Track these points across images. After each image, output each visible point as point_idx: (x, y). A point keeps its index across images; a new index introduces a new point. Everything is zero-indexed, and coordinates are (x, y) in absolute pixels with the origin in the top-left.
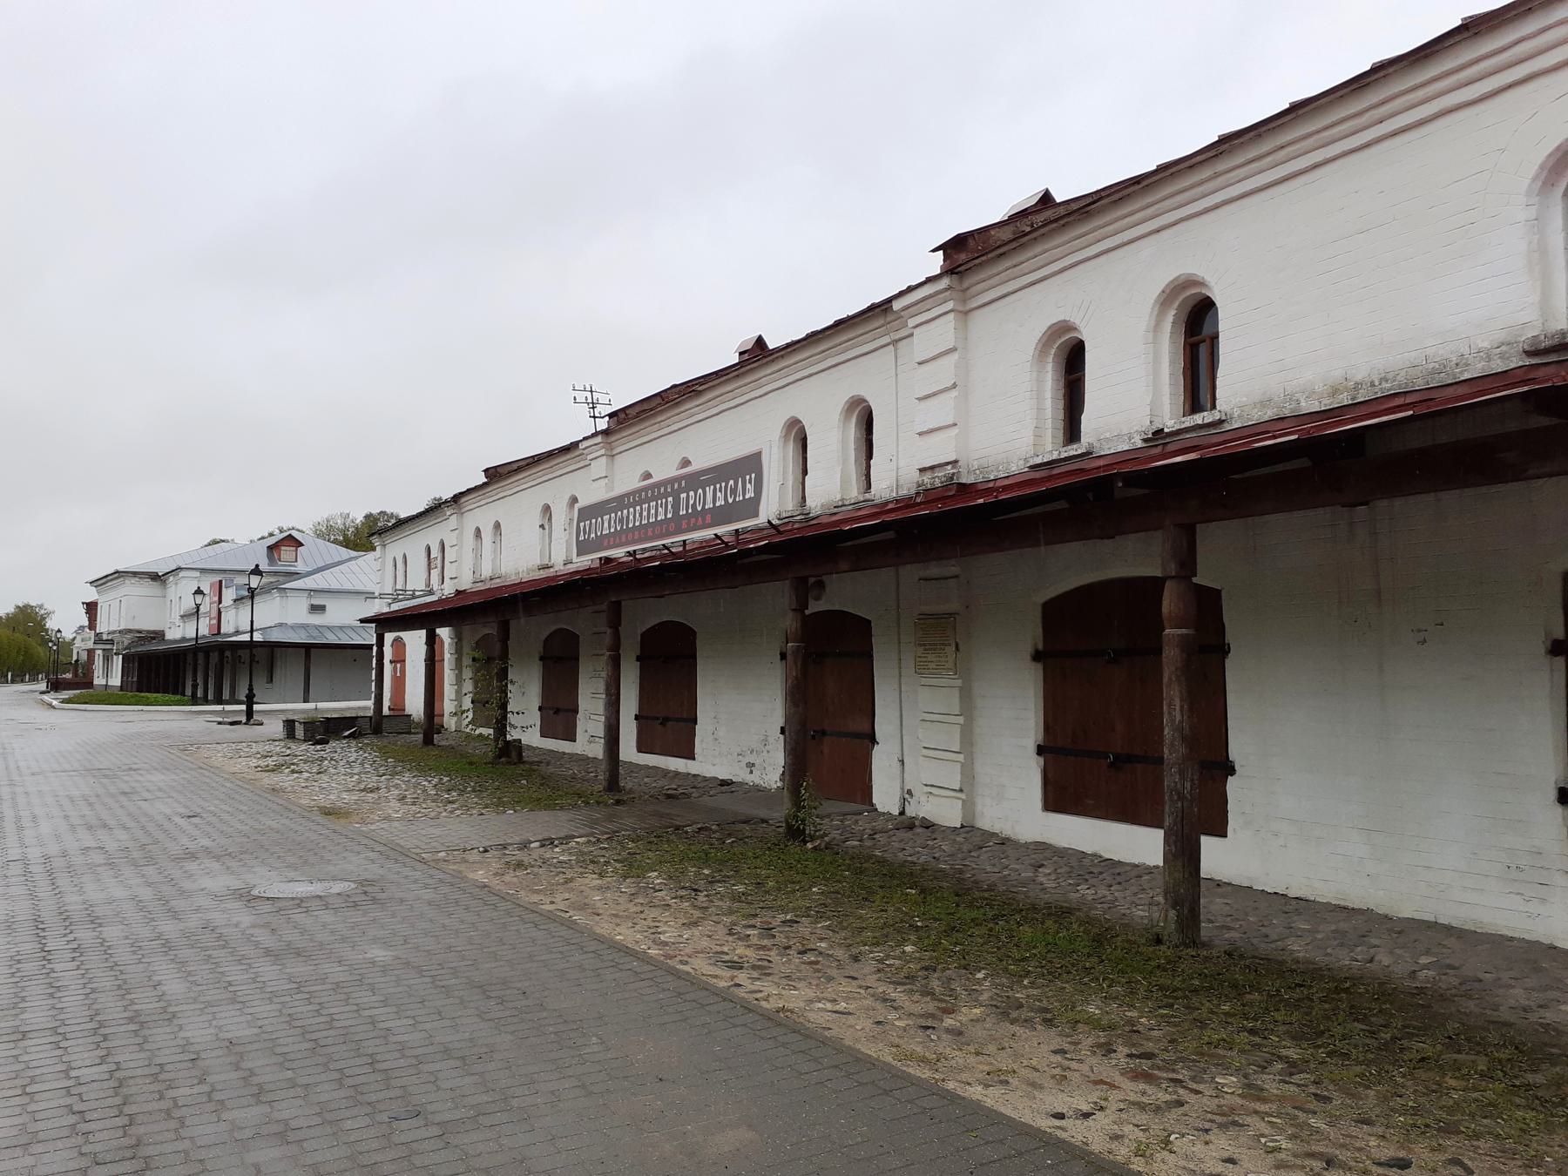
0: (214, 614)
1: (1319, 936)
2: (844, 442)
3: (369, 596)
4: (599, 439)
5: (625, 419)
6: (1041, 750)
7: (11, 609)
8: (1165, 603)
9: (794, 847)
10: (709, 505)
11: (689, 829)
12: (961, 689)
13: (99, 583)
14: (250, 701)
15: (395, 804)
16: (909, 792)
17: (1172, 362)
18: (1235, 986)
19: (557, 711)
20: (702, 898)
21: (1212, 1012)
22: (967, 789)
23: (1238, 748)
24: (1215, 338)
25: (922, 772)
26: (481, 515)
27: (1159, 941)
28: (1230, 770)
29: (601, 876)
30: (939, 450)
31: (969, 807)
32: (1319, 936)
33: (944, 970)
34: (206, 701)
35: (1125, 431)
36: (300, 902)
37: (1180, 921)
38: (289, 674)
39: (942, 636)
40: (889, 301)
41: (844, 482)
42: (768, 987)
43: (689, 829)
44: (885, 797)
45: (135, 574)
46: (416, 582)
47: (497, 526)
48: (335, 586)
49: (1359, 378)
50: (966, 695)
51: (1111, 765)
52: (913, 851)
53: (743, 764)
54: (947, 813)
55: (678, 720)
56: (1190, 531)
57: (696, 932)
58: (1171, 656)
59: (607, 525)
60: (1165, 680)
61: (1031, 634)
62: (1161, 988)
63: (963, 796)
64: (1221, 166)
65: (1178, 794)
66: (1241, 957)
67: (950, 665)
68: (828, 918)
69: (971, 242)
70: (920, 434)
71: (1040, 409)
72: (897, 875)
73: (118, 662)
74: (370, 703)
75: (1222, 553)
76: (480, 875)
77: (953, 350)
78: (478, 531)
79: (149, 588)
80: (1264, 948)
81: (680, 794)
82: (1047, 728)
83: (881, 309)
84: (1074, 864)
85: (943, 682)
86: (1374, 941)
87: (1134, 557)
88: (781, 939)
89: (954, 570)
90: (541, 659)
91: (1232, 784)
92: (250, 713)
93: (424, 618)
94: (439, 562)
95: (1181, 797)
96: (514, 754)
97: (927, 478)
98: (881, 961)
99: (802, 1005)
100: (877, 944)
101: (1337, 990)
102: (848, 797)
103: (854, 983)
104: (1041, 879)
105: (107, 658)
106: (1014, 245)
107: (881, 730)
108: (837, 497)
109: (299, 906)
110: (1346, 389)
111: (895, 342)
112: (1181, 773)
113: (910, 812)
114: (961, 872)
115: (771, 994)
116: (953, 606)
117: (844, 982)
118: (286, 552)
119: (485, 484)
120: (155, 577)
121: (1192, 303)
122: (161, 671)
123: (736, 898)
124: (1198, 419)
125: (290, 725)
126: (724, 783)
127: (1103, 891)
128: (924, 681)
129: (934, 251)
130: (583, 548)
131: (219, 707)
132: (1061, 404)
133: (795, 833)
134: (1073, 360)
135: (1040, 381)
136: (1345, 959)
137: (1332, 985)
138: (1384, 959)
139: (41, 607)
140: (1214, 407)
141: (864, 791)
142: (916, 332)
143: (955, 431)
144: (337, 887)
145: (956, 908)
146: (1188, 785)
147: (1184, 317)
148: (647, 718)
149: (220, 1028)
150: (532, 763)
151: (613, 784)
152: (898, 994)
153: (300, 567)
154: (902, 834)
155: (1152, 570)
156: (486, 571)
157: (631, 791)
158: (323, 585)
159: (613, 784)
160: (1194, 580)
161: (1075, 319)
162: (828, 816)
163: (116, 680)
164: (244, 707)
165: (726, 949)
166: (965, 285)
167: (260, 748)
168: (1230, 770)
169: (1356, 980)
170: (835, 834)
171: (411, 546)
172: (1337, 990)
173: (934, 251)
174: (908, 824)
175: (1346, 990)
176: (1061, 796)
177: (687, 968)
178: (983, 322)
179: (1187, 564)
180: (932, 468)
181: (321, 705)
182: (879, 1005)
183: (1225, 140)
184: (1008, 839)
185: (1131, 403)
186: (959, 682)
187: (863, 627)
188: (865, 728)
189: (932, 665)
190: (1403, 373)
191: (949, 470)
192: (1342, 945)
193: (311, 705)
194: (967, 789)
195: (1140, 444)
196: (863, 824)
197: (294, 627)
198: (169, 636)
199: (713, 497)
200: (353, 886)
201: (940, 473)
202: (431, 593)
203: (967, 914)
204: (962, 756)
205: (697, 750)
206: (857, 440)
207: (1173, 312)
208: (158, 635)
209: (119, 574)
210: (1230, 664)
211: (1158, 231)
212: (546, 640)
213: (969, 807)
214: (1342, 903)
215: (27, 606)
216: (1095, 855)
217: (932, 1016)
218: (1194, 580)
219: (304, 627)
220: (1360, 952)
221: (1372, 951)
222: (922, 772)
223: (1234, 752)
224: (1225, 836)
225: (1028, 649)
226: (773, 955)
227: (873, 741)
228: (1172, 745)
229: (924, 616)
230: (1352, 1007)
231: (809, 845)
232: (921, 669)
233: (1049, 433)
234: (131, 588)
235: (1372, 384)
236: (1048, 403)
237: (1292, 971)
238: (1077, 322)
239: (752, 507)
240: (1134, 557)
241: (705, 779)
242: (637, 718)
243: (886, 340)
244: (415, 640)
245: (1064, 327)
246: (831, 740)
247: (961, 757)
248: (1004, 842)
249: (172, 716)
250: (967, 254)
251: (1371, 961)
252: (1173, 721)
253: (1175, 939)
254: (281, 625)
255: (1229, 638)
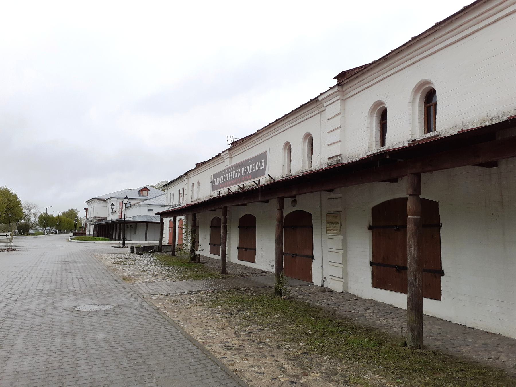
0: (120, 212)
1: (477, 345)
2: (303, 149)
3: (164, 206)
4: (227, 152)
5: (235, 144)
6: (371, 264)
7: (67, 211)
8: (408, 205)
9: (277, 298)
10: (251, 172)
11: (242, 289)
12: (342, 240)
13: (88, 202)
14: (124, 240)
15: (149, 276)
16: (325, 278)
17: (420, 114)
18: (433, 369)
19: (215, 245)
20: (232, 317)
21: (420, 382)
22: (345, 277)
23: (445, 265)
24: (435, 104)
25: (329, 271)
26: (194, 179)
27: (405, 345)
28: (443, 274)
29: (201, 306)
30: (334, 151)
31: (345, 284)
32: (477, 345)
33: (312, 354)
34: (115, 240)
35: (402, 141)
36: (89, 313)
37: (414, 337)
38: (141, 232)
39: (336, 220)
40: (317, 97)
41: (303, 163)
42: (237, 359)
43: (242, 289)
44: (317, 280)
45: (98, 199)
46: (176, 202)
47: (198, 182)
48: (156, 203)
49: (493, 115)
50: (344, 242)
51: (397, 270)
52: (321, 301)
53: (270, 265)
54: (337, 286)
55: (250, 249)
56: (418, 176)
57: (222, 332)
58: (410, 227)
59: (221, 180)
60: (408, 237)
61: (368, 219)
62: (401, 368)
63: (343, 280)
64: (437, 36)
65: (413, 284)
66: (440, 354)
67: (338, 231)
68: (276, 329)
69: (347, 75)
70: (328, 145)
71: (371, 134)
72: (310, 310)
73: (93, 227)
74: (158, 242)
75: (435, 187)
76: (159, 305)
77: (340, 114)
78: (193, 184)
79: (102, 204)
80: (452, 350)
81: (246, 275)
82: (373, 256)
83: (314, 101)
84: (381, 308)
85: (337, 237)
86: (501, 349)
87: (401, 190)
88: (253, 337)
89: (340, 195)
90: (210, 227)
91: (443, 279)
92: (124, 244)
93: (173, 213)
94: (182, 195)
95: (414, 285)
96: (197, 260)
97: (330, 161)
98: (288, 349)
99: (246, 368)
100: (290, 341)
101: (479, 373)
102: (304, 279)
103: (273, 359)
104: (366, 315)
105: (90, 226)
106: (360, 73)
107: (317, 253)
108: (300, 169)
109: (88, 314)
110: (488, 120)
111: (321, 112)
112: (415, 275)
113: (325, 286)
114: (335, 311)
115: (236, 362)
116: (340, 209)
117: (268, 357)
118: (144, 193)
119: (195, 169)
120: (104, 200)
121: (427, 91)
122: (107, 230)
123: (244, 318)
124: (429, 135)
125: (132, 248)
126: (263, 272)
127: (390, 321)
128: (330, 237)
129: (334, 78)
130: (214, 188)
131: (118, 242)
132: (379, 132)
133: (279, 293)
134: (383, 115)
135: (371, 124)
136: (485, 358)
137: (477, 371)
138: (503, 358)
139: (76, 210)
140: (435, 131)
141: (309, 277)
142: (327, 108)
143: (340, 144)
144: (106, 307)
145: (331, 326)
146: (417, 281)
147: (424, 96)
148: (241, 248)
149: (101, 351)
150: (202, 263)
151: (224, 271)
152: (287, 365)
153: (149, 197)
154: (321, 294)
155: (404, 195)
156: (195, 198)
157: (230, 274)
158: (152, 203)
159: (224, 271)
160: (421, 196)
161: (383, 100)
162: (295, 286)
163: (92, 233)
164: (122, 242)
165: (229, 340)
166: (344, 89)
167: (120, 256)
168: (443, 274)
169: (489, 369)
170: (295, 293)
171: (175, 189)
172: (479, 373)
173: (334, 78)
174: (323, 290)
175: (483, 374)
176: (379, 282)
177: (209, 348)
178: (352, 103)
179: (417, 190)
180: (332, 157)
181: (150, 242)
182: (278, 370)
183: (438, 25)
184: (359, 298)
185: (405, 130)
186: (342, 237)
187: (310, 215)
188: (311, 254)
189: (332, 231)
190: (511, 112)
191: (338, 158)
192: (486, 350)
193: (147, 242)
194: (345, 277)
195: (407, 145)
196: (307, 290)
197: (143, 216)
198: (108, 219)
199: (252, 169)
200: (112, 307)
201: (335, 159)
202: (180, 205)
203: (330, 329)
204: (343, 265)
205: (256, 260)
206: (308, 149)
207: (420, 95)
208: (105, 219)
209: (93, 199)
210: (442, 231)
211: (413, 64)
212: (212, 221)
213: (345, 284)
214: (489, 331)
215: (72, 210)
216: (391, 305)
217: (297, 376)
218: (421, 196)
219: (146, 216)
220: (493, 354)
221: (499, 354)
222: (329, 271)
223: (444, 267)
224: (440, 299)
225: (366, 225)
226: (247, 345)
227: (313, 258)
228: (411, 264)
229: (329, 212)
230: (485, 383)
231: (282, 297)
232: (328, 232)
233: (374, 143)
234: (97, 204)
235: (499, 118)
236: (374, 132)
237: (461, 363)
238: (384, 101)
239: (262, 172)
240: (401, 190)
241: (258, 270)
242: (238, 248)
243: (317, 112)
244: (167, 221)
245: (379, 103)
246: (296, 258)
247: (342, 266)
248: (357, 298)
249: (103, 245)
250: (345, 78)
251: (498, 359)
252: (411, 254)
253: (412, 344)
254: (139, 215)
255: (442, 221)
